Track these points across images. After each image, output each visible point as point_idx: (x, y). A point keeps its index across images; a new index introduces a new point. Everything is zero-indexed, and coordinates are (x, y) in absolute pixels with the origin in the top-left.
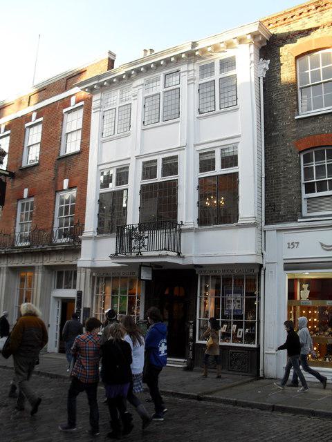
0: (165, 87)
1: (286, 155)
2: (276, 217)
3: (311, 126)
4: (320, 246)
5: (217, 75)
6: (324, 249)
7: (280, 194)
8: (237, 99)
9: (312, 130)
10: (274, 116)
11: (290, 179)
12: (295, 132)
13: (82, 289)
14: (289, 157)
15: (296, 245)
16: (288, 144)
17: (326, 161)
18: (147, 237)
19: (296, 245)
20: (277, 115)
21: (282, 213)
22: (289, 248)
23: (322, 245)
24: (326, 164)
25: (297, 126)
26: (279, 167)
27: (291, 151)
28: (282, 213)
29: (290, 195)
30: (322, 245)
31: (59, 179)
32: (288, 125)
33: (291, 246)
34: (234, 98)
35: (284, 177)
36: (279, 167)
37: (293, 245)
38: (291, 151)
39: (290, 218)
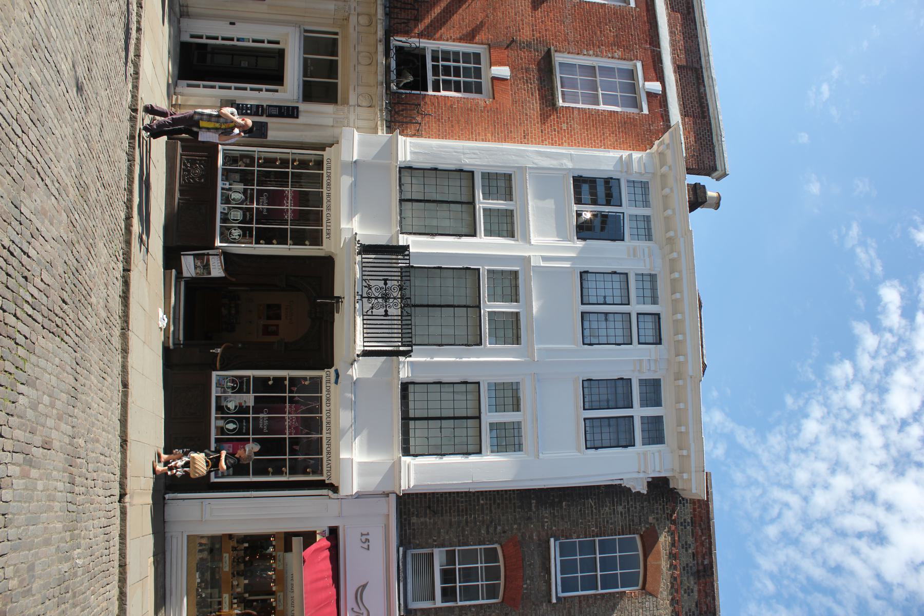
0: (638, 314)
1: (499, 525)
2: (409, 511)
3: (537, 561)
4: (363, 583)
5: (638, 412)
6: (360, 587)
7: (442, 516)
8: (596, 448)
9: (530, 565)
10: (560, 502)
11: (463, 530)
12: (531, 537)
13: (302, 119)
14: (496, 528)
15: (365, 546)
16: (515, 526)
17: (484, 565)
18: (386, 314)
19: (365, 546)
20: (562, 507)
21: (414, 520)
22: (362, 535)
23: (364, 586)
24: (479, 565)
25: (539, 540)
26: (483, 513)
27: (504, 532)
28: (414, 520)
29: (439, 533)
30: (364, 586)
31: (512, 53)
32: (543, 526)
33: (364, 538)
34: (598, 444)
35: (467, 522)
36: (483, 513)
37: (366, 541)
38: (504, 532)
39: (405, 535)
